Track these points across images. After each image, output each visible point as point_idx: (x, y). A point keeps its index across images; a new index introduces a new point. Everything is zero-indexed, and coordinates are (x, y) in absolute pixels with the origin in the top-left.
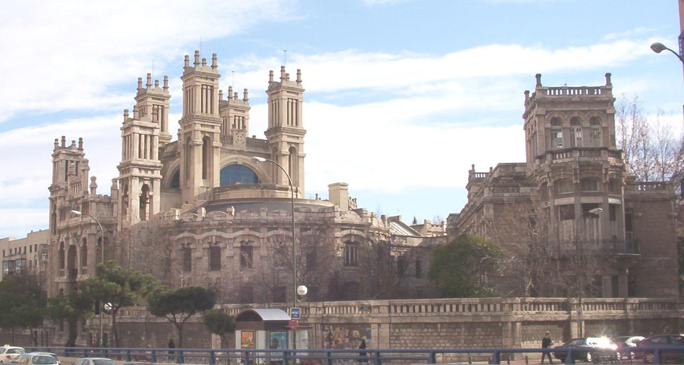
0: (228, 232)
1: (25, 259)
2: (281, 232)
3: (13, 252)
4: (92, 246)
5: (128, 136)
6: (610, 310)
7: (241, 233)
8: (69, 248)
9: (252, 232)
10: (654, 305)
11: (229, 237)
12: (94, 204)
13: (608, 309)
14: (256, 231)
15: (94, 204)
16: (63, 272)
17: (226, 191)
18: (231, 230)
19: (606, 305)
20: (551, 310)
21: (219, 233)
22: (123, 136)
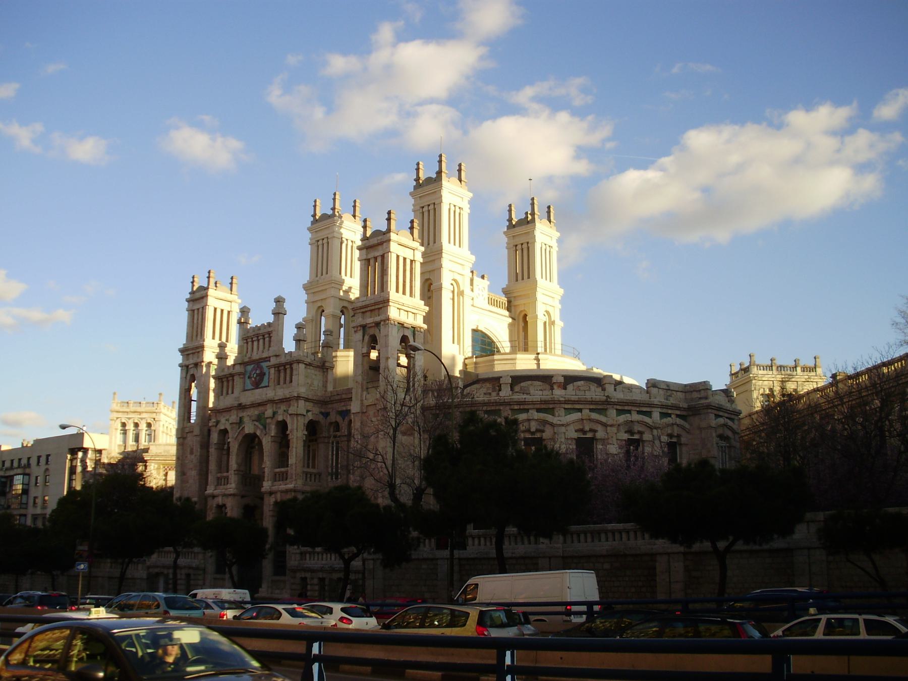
0: (557, 414)
1: (29, 475)
2: (635, 417)
3: (16, 464)
4: (297, 434)
5: (376, 258)
6: (593, 541)
7: (576, 416)
8: (240, 438)
9: (595, 416)
10: (308, 556)
11: (559, 423)
12: (302, 366)
13: (513, 543)
14: (600, 414)
15: (302, 366)
16: (227, 478)
17: (85, 604)
18: (562, 412)
19: (606, 534)
20: (600, 540)
21: (542, 416)
22: (365, 257)
